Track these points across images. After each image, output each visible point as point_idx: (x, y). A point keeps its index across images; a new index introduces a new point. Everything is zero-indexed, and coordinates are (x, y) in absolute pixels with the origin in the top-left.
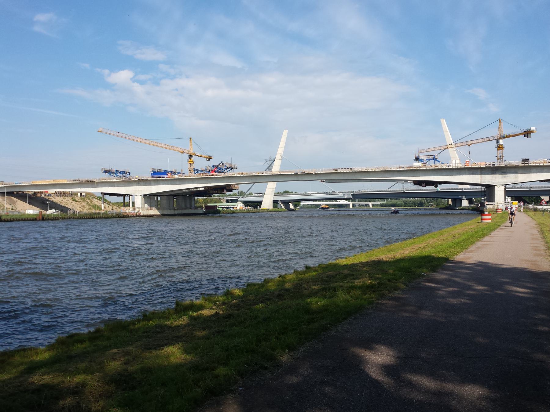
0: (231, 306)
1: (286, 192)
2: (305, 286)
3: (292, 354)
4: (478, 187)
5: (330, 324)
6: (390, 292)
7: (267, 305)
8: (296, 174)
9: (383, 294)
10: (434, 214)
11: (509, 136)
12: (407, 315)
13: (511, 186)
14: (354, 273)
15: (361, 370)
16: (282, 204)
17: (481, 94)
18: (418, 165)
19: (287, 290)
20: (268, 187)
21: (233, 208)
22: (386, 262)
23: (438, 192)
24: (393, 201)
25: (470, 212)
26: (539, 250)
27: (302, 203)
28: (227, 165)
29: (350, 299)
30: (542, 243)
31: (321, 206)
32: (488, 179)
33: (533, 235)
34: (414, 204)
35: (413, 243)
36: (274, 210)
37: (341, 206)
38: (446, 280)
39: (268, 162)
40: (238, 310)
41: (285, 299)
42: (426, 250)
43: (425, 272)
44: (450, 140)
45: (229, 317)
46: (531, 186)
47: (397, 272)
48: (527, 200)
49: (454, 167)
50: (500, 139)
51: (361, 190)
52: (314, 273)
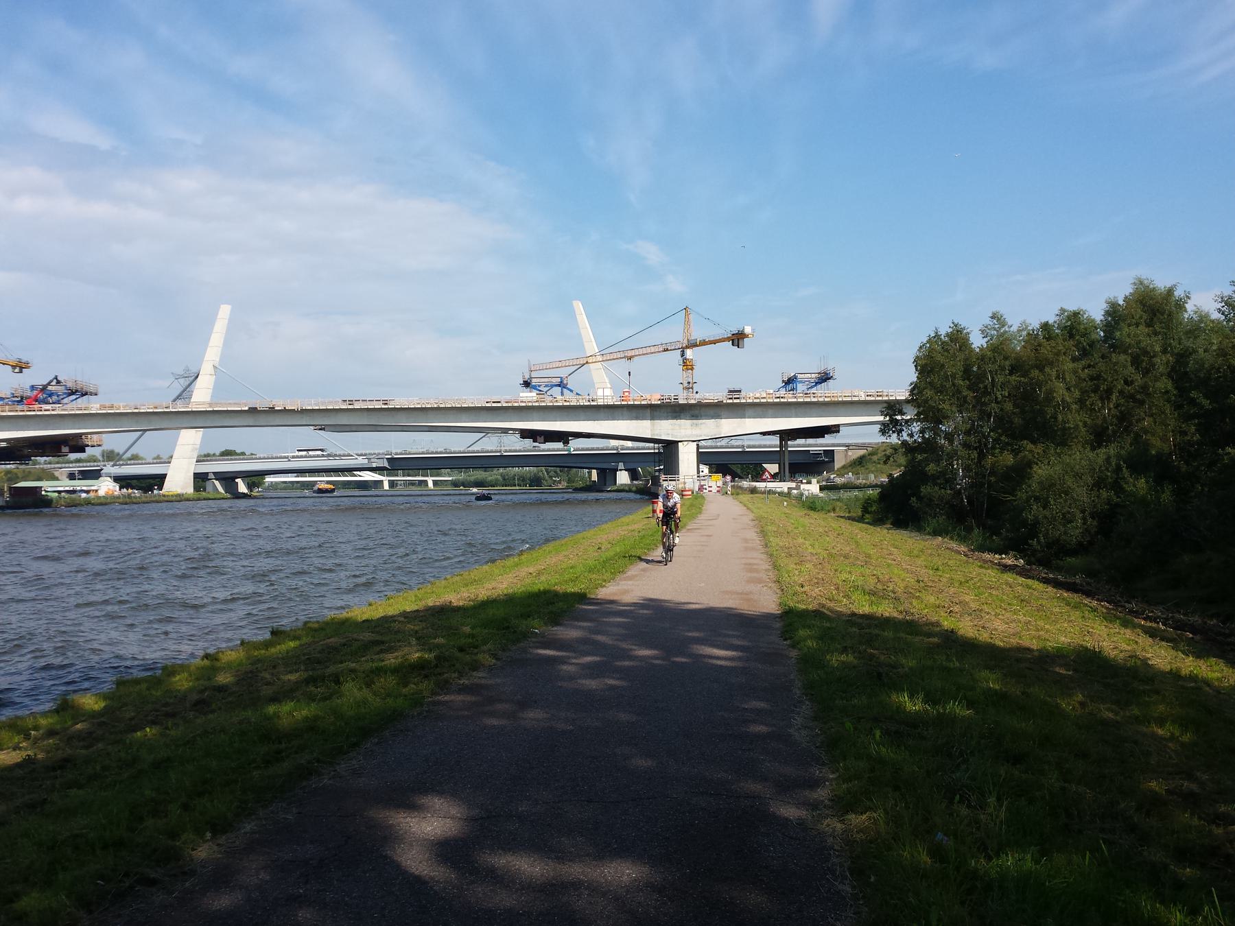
0: (70, 739)
1: (228, 454)
2: (268, 676)
3: (222, 840)
4: (648, 445)
5: (318, 761)
6: (461, 676)
7: (167, 728)
8: (253, 411)
9: (446, 682)
10: (562, 503)
11: (704, 343)
12: (494, 722)
13: (709, 443)
14: (385, 638)
15: (386, 857)
16: (217, 483)
17: (652, 253)
18: (529, 397)
19: (221, 689)
20: (180, 441)
21: (87, 492)
22: (458, 609)
23: (570, 455)
24: (479, 475)
25: (632, 495)
26: (757, 571)
27: (269, 479)
28: (70, 385)
29: (370, 697)
30: (764, 556)
31: (316, 488)
32: (666, 429)
33: (746, 540)
34: (523, 480)
35: (517, 565)
36: (197, 495)
37: (364, 485)
38: (584, 641)
39: (182, 381)
40: (87, 747)
41: (213, 712)
42: (543, 578)
43: (537, 627)
44: (592, 347)
45: (64, 764)
46: (746, 443)
47: (478, 630)
48: (739, 471)
49: (600, 402)
50: (687, 347)
51: (409, 450)
52: (292, 644)
